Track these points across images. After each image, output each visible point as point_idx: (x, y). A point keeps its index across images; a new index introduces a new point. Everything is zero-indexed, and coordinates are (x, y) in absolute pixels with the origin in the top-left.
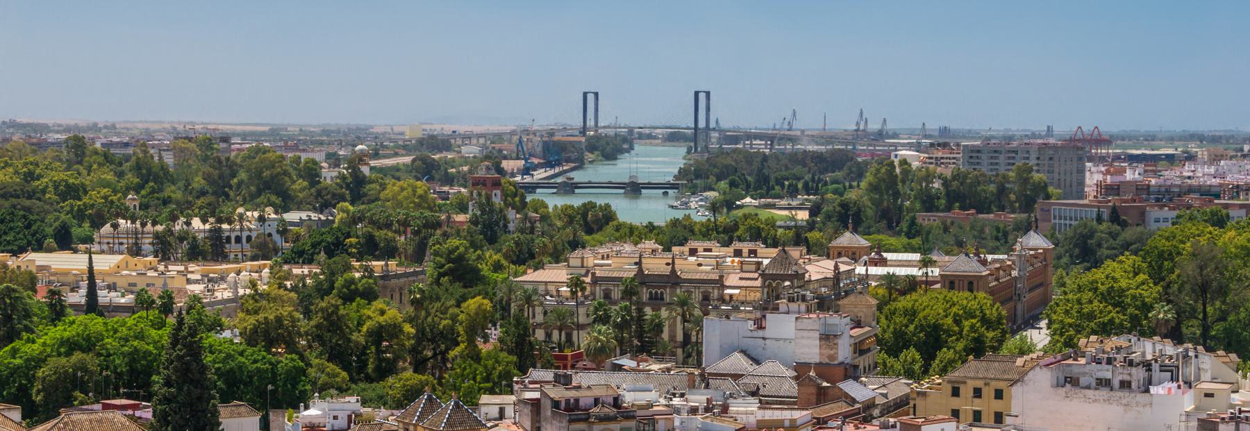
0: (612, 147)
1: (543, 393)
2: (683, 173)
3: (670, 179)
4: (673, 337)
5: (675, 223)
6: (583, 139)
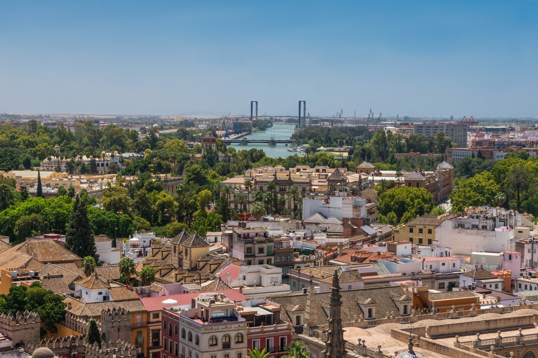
0: (263, 125)
1: (234, 231)
2: (294, 136)
3: (289, 139)
4: (289, 207)
5: (290, 158)
6: (251, 122)
